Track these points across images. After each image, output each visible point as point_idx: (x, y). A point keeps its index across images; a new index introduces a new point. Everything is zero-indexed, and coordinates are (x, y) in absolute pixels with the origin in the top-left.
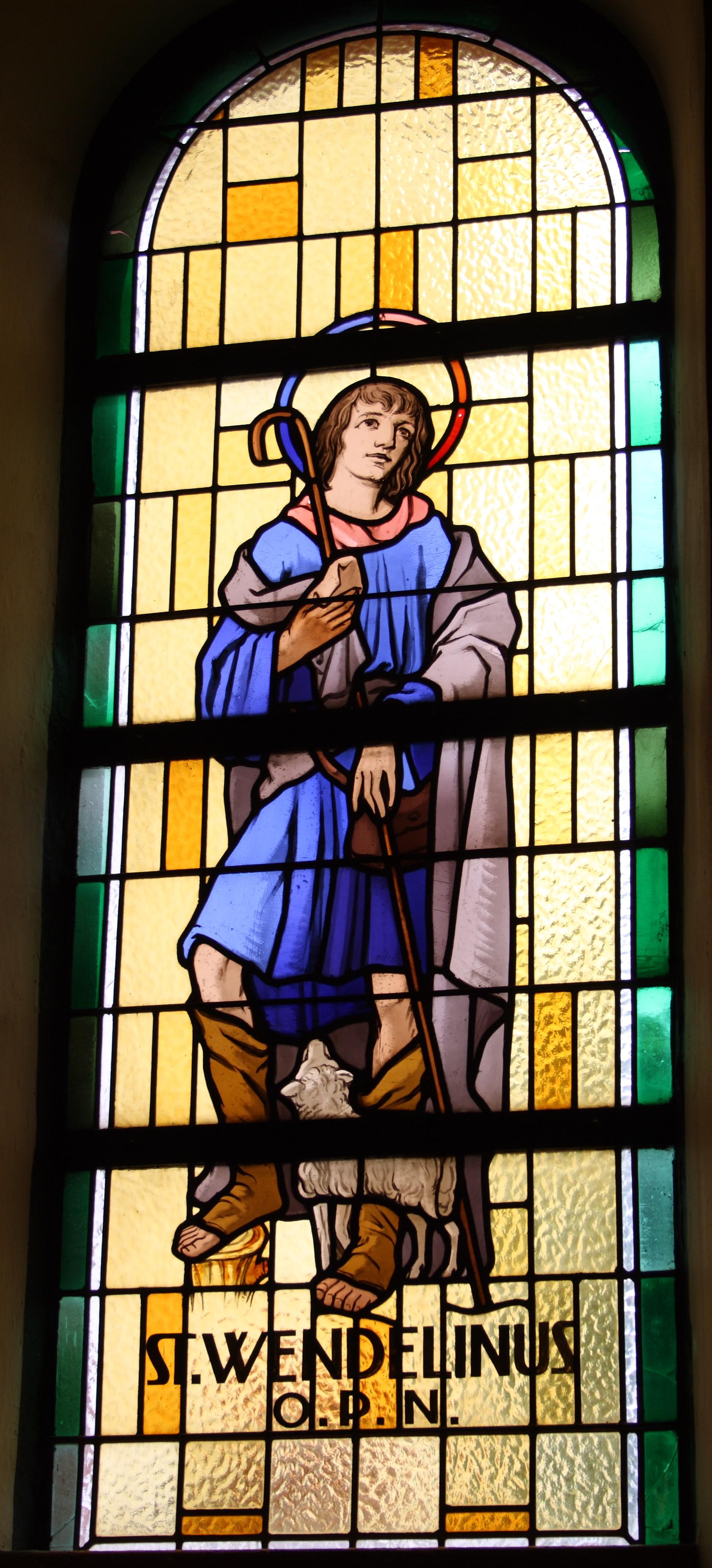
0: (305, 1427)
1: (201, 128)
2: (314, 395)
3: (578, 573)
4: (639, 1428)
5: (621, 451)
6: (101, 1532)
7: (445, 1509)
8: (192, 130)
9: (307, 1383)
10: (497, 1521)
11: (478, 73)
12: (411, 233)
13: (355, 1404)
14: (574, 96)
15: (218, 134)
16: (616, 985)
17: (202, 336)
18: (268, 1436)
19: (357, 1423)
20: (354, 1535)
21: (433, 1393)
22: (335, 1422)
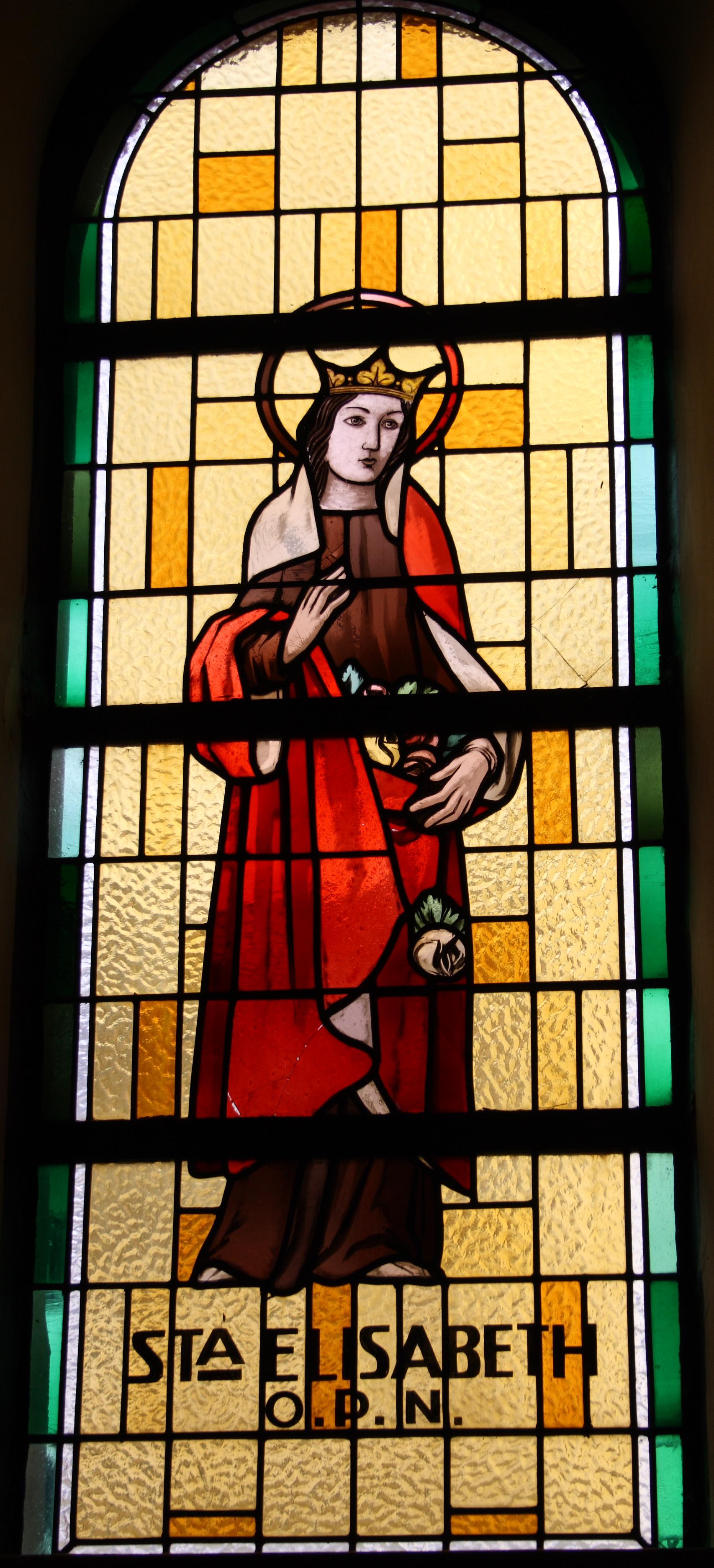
0: (301, 1425)
1: (172, 96)
2: (297, 373)
3: (577, 566)
4: (652, 1432)
5: (619, 444)
6: (81, 1534)
7: (169, 1514)
8: (160, 100)
10: (227, 1528)
11: (465, 52)
12: (394, 213)
15: (188, 105)
16: (621, 985)
17: (175, 308)
18: (260, 1436)
19: (354, 1424)
21: (434, 1394)
22: (330, 1422)
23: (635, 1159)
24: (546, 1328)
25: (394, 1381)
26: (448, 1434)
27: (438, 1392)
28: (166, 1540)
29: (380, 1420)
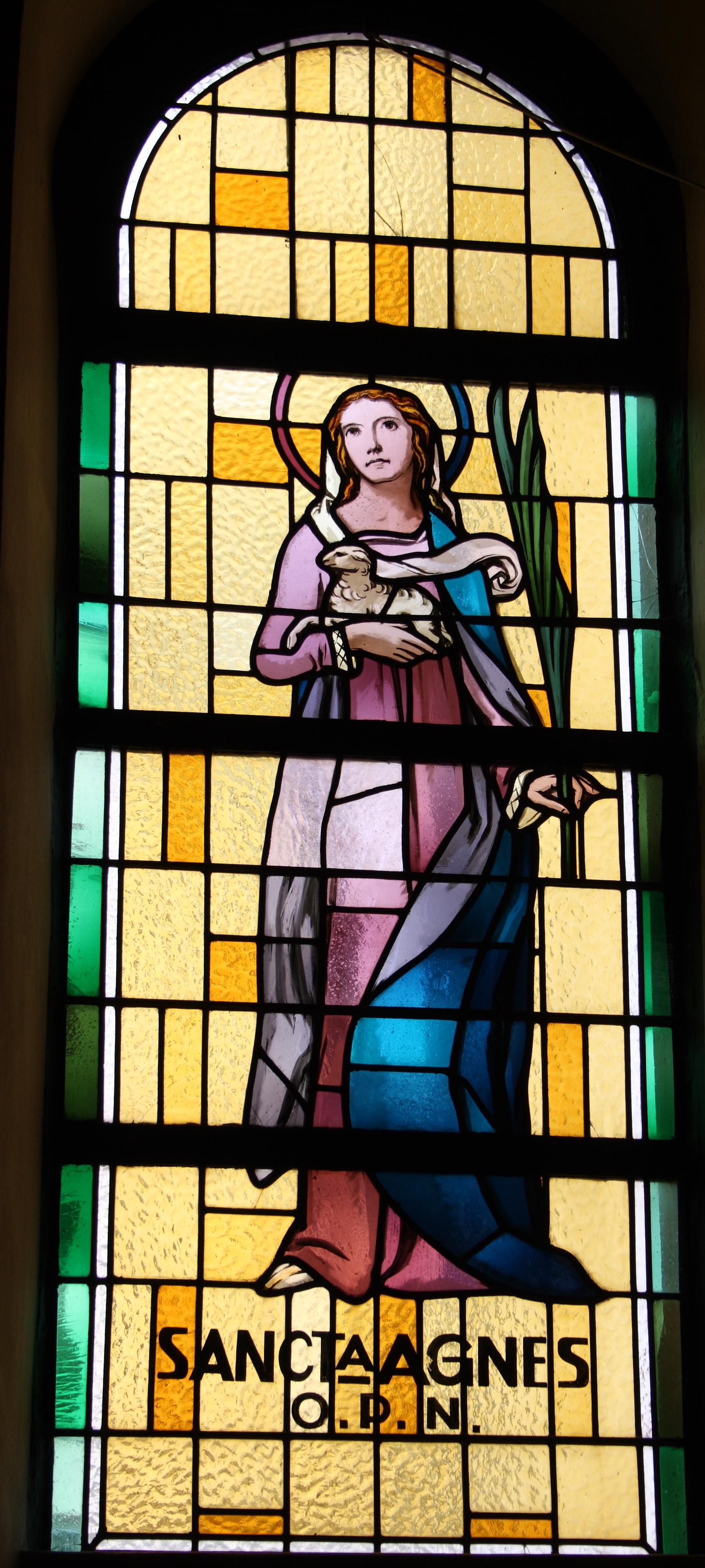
0: (323, 1429)
1: (186, 108)
2: (314, 396)
9: (326, 1385)
11: (473, 103)
13: (375, 1410)
14: (568, 147)
19: (377, 1428)
20: (378, 1539)
22: (354, 1426)
23: (639, 1186)
24: (342, 1336)
25: (191, 1384)
26: (465, 1440)
27: (457, 1399)
28: (467, 1540)
29: (401, 1425)
